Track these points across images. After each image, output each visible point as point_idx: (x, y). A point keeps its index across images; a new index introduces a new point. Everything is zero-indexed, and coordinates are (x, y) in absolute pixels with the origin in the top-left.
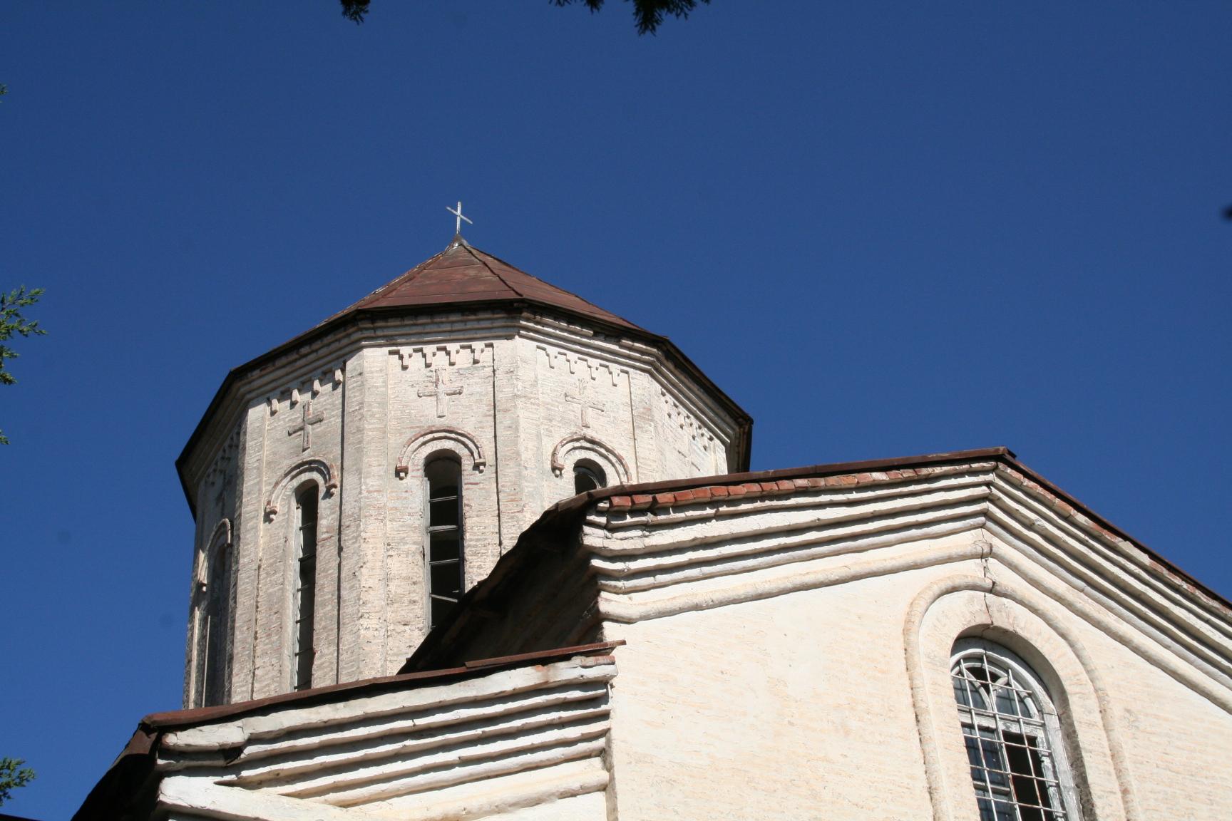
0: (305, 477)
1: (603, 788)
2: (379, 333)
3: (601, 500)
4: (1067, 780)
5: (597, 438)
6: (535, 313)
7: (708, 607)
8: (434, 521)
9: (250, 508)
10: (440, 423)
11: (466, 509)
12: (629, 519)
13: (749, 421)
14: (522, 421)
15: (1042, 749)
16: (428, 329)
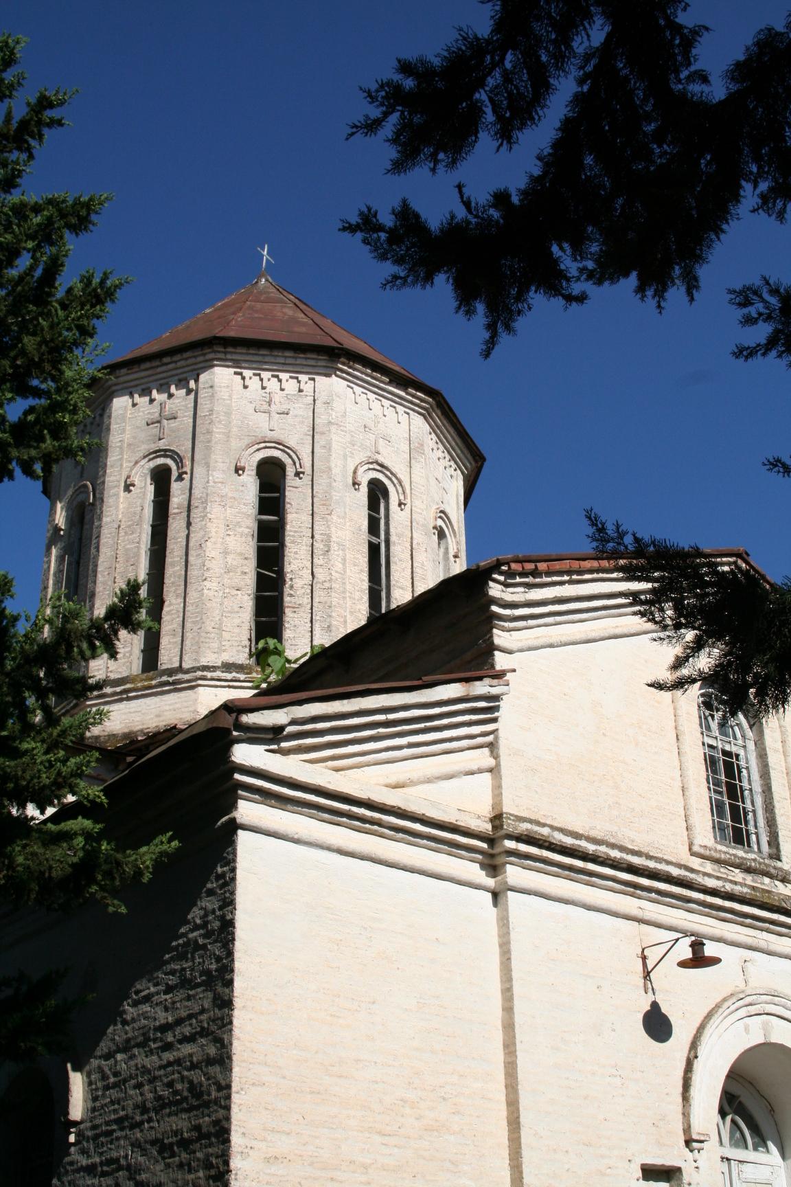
0: (169, 462)
1: (490, 770)
2: (229, 357)
3: (503, 564)
4: (757, 786)
5: (386, 463)
6: (349, 360)
8: (261, 512)
9: (112, 479)
10: (270, 435)
11: (288, 506)
12: (518, 580)
13: (483, 459)
14: (334, 445)
15: (742, 763)
16: (267, 359)
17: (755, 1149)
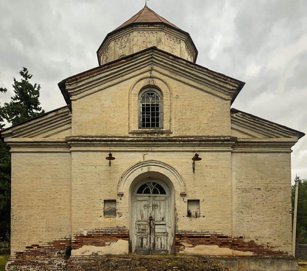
7: (91, 94)
17: (161, 194)
